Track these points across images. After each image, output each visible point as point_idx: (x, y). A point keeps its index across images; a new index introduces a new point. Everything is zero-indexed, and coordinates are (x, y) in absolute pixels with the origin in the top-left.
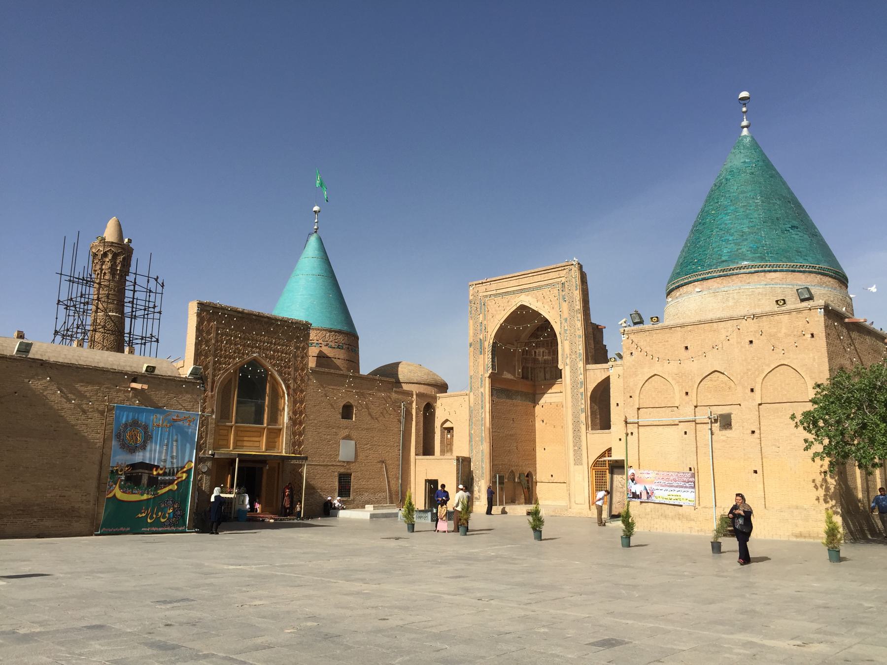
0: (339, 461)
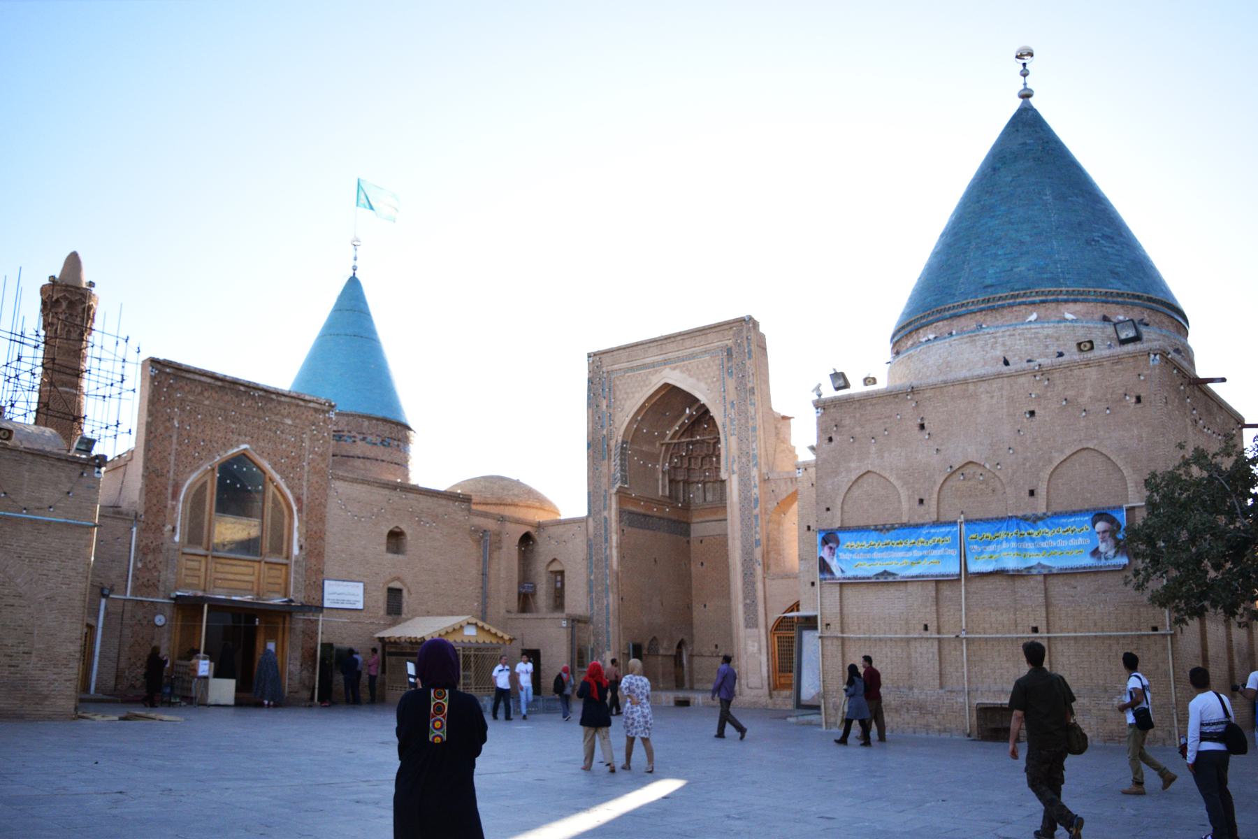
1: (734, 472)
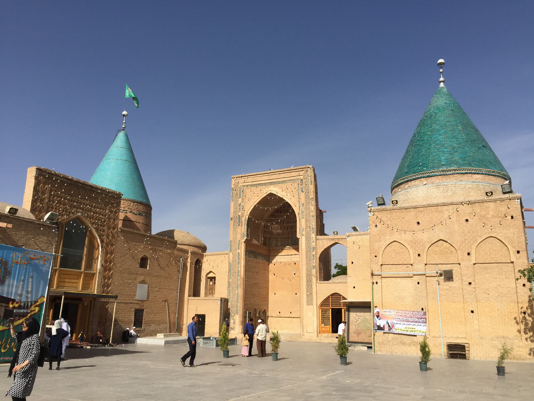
0: (136, 300)
1: (303, 235)
